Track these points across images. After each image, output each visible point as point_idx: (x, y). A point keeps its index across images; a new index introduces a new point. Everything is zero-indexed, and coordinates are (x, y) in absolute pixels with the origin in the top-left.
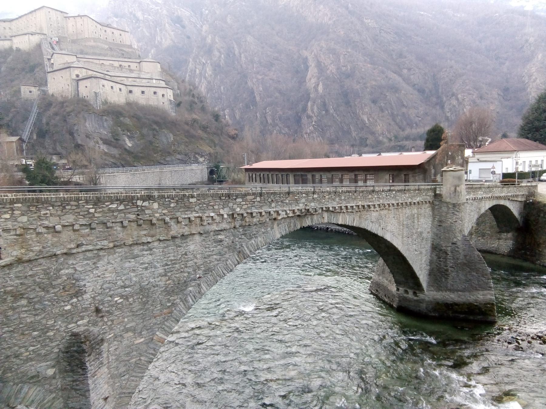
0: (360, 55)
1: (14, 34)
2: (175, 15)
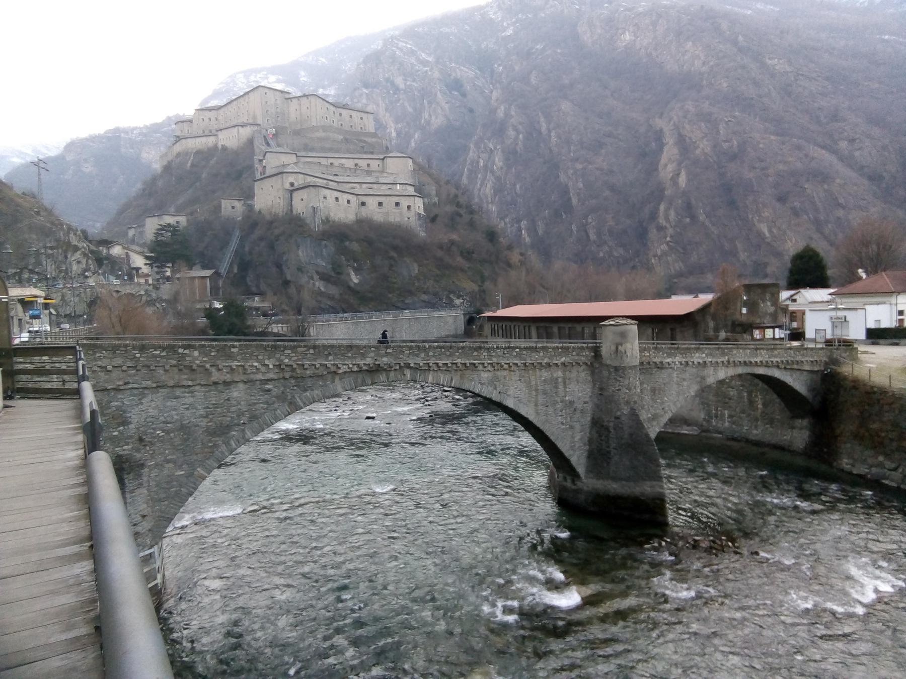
0: (757, 120)
1: (222, 127)
2: (452, 77)
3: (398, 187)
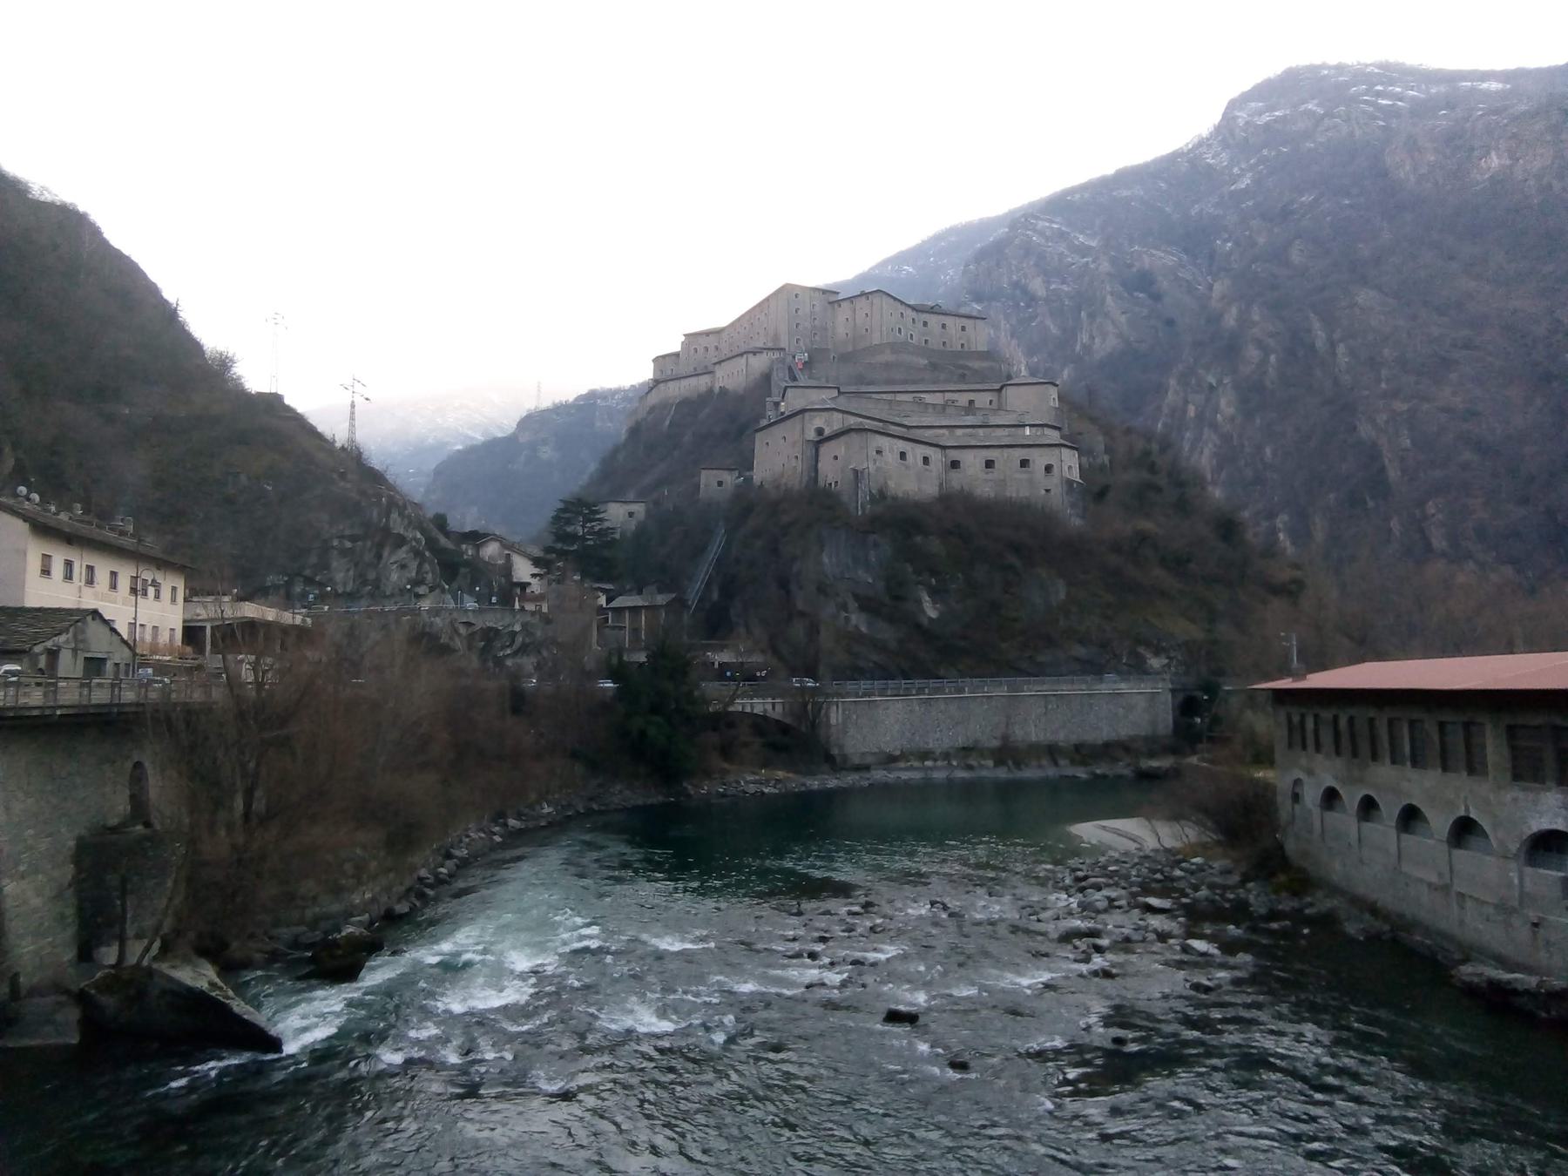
3: (1027, 431)
